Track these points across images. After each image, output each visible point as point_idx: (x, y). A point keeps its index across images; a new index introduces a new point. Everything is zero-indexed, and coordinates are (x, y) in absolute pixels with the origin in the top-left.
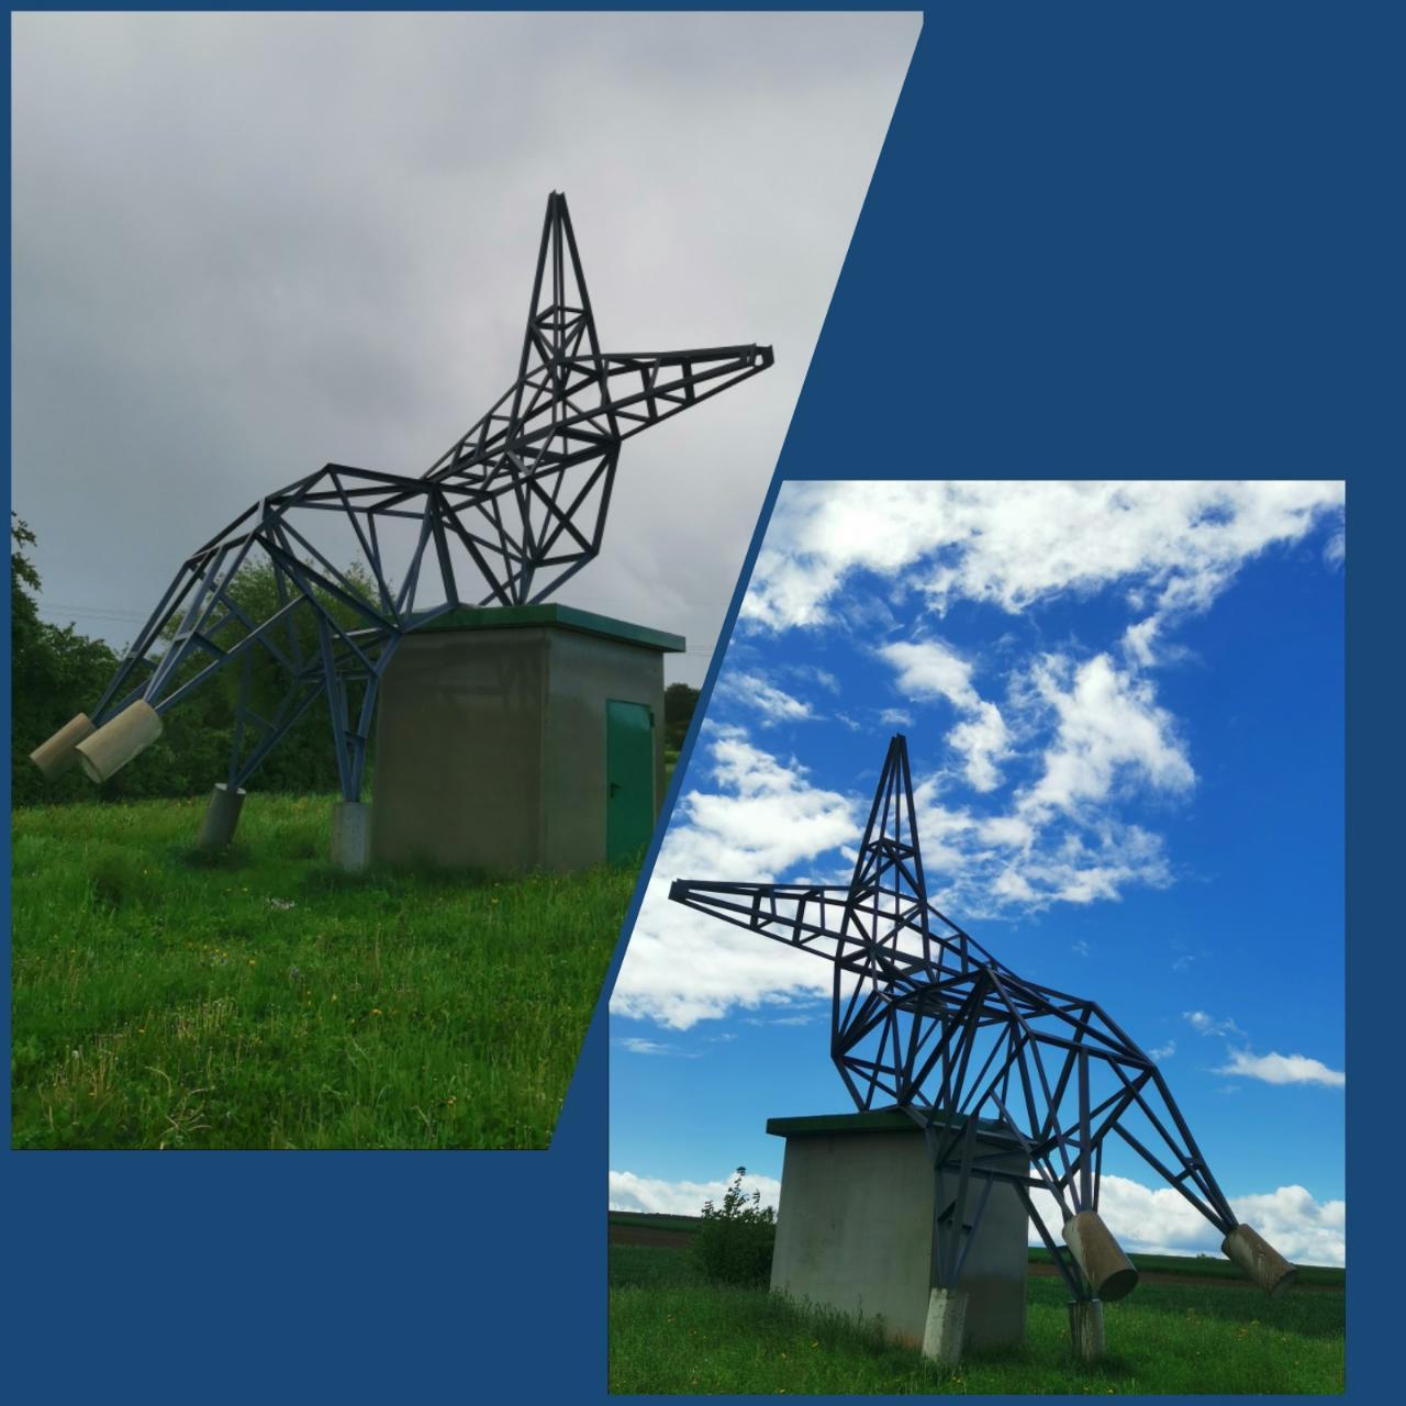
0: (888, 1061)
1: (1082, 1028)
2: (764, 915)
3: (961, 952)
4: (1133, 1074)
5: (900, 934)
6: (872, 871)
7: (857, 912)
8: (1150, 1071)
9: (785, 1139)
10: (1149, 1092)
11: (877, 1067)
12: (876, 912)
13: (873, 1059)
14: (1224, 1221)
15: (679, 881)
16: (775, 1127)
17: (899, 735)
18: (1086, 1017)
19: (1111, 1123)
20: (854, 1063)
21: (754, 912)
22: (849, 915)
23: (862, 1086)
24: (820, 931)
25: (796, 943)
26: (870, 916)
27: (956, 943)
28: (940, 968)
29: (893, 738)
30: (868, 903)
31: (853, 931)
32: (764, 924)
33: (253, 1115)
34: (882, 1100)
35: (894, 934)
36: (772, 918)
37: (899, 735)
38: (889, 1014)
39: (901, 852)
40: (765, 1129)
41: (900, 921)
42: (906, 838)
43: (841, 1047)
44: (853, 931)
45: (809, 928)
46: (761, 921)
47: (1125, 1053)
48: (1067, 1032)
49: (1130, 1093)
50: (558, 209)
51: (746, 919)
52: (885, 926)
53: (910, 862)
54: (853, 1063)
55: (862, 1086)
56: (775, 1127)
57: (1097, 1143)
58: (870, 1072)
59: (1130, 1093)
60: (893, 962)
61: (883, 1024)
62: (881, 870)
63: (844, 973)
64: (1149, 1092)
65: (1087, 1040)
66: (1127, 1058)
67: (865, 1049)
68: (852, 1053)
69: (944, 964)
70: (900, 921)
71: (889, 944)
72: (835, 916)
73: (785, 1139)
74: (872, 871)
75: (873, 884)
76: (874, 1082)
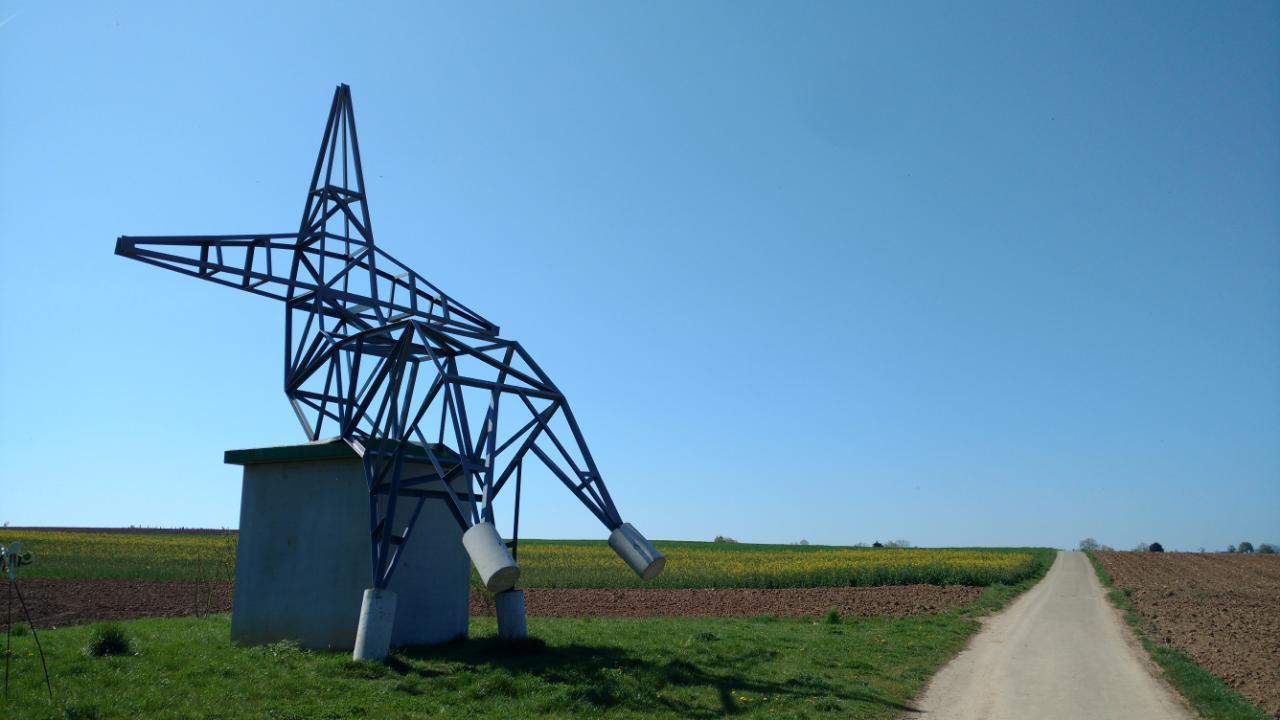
0: (333, 392)
1: (505, 368)
2: (211, 266)
3: (411, 286)
4: (542, 404)
5: (351, 272)
6: (319, 216)
7: (307, 255)
8: (560, 401)
10: (557, 422)
11: (325, 398)
12: (323, 253)
13: (321, 391)
14: (608, 514)
15: (124, 237)
16: (232, 457)
17: (342, 84)
18: (508, 357)
19: (530, 444)
20: (304, 396)
21: (203, 263)
22: (299, 257)
24: (267, 278)
25: (246, 286)
26: (318, 257)
27: (406, 280)
28: (391, 306)
29: (338, 88)
30: (316, 245)
31: (304, 275)
32: (212, 273)
33: (1112, 576)
34: (331, 431)
35: (345, 273)
36: (220, 267)
37: (342, 84)
38: (334, 355)
39: (312, 301)
40: (228, 449)
41: (350, 261)
42: (353, 187)
43: (293, 390)
44: (304, 275)
45: (257, 275)
46: (208, 271)
47: (546, 389)
48: (491, 374)
49: (541, 421)
51: (196, 269)
52: (333, 267)
53: (355, 207)
54: (303, 396)
55: (312, 415)
56: (232, 457)
57: (516, 463)
58: (318, 403)
59: (541, 421)
60: (345, 304)
61: (328, 362)
62: (327, 216)
63: (295, 312)
64: (557, 422)
65: (510, 380)
66: (543, 392)
67: (314, 383)
68: (304, 387)
69: (396, 302)
70: (350, 261)
71: (338, 286)
72: (282, 262)
74: (319, 216)
75: (319, 229)
76: (323, 411)
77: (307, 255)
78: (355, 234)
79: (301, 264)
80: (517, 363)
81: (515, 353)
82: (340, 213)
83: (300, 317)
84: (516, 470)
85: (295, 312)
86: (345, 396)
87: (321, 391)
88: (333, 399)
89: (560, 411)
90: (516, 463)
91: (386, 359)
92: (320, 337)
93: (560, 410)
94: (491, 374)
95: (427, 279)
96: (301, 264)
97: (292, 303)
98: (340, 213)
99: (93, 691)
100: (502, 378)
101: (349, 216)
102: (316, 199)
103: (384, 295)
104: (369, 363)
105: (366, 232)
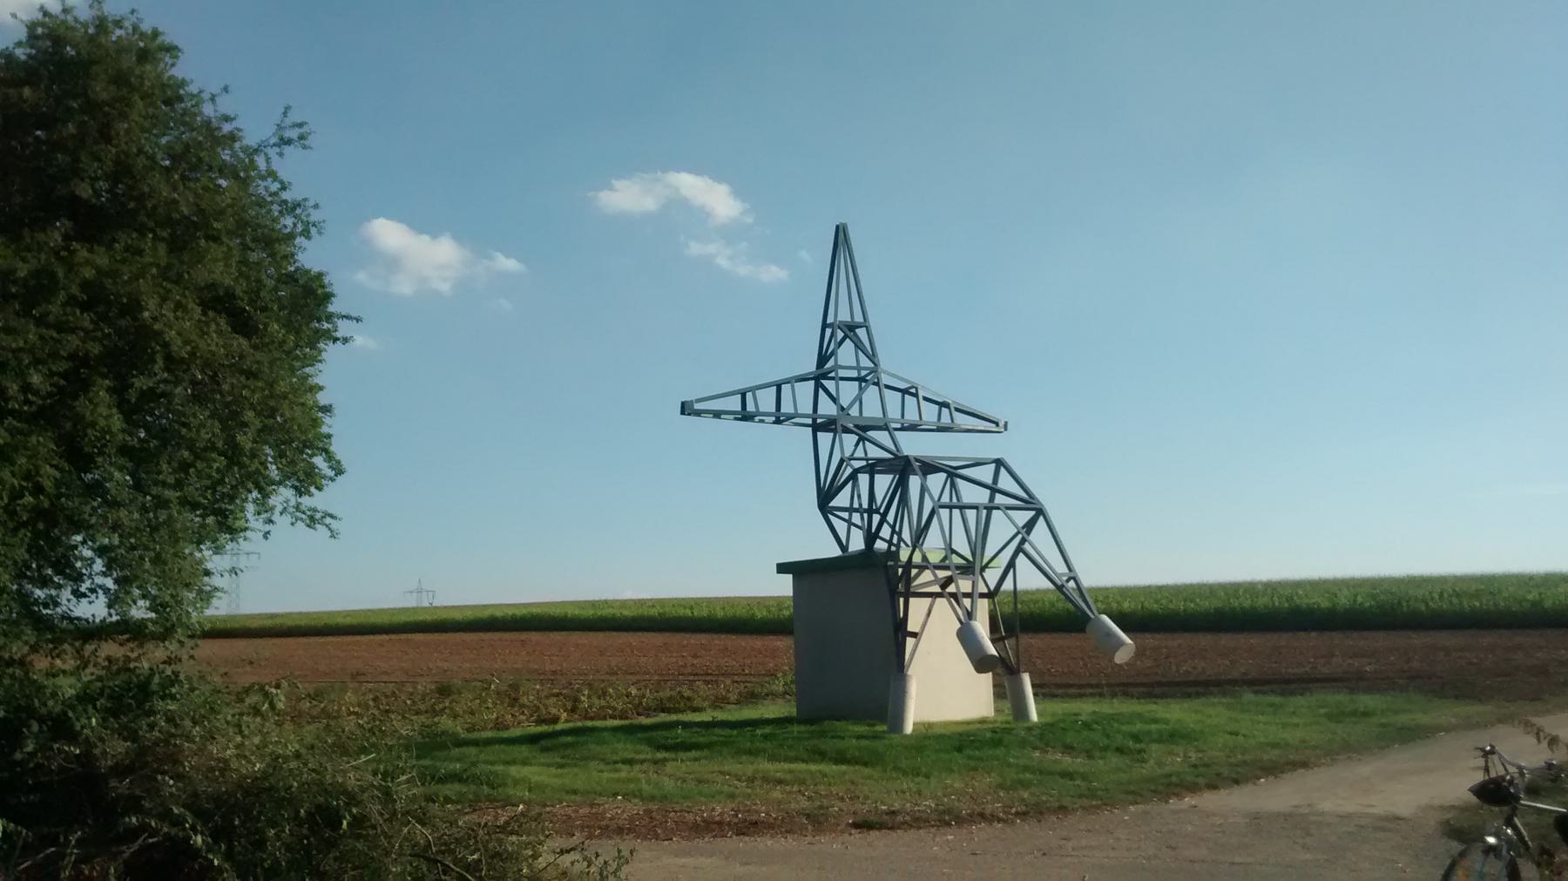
1: (994, 490)
4: (1023, 517)
7: (825, 382)
8: (1040, 512)
9: (791, 576)
11: (851, 510)
13: (848, 505)
16: (783, 568)
22: (818, 386)
23: (841, 527)
34: (857, 543)
42: (859, 318)
43: (825, 497)
47: (1029, 502)
50: (841, 237)
52: (848, 392)
53: (861, 332)
56: (783, 568)
57: (1011, 565)
58: (845, 515)
63: (820, 434)
65: (999, 499)
67: (842, 500)
73: (791, 576)
76: (850, 523)
77: (825, 382)
78: (865, 362)
79: (821, 391)
80: (1006, 482)
81: (1002, 469)
82: (848, 344)
83: (825, 438)
84: (1012, 570)
85: (820, 434)
86: (865, 506)
87: (848, 505)
88: (856, 510)
89: (1041, 520)
90: (1011, 565)
91: (897, 476)
92: (842, 461)
93: (1041, 518)
94: (982, 496)
95: (922, 412)
96: (821, 391)
97: (816, 428)
98: (848, 344)
99: (193, 532)
100: (992, 499)
101: (858, 346)
102: (828, 332)
103: (894, 412)
104: (884, 482)
105: (872, 357)
